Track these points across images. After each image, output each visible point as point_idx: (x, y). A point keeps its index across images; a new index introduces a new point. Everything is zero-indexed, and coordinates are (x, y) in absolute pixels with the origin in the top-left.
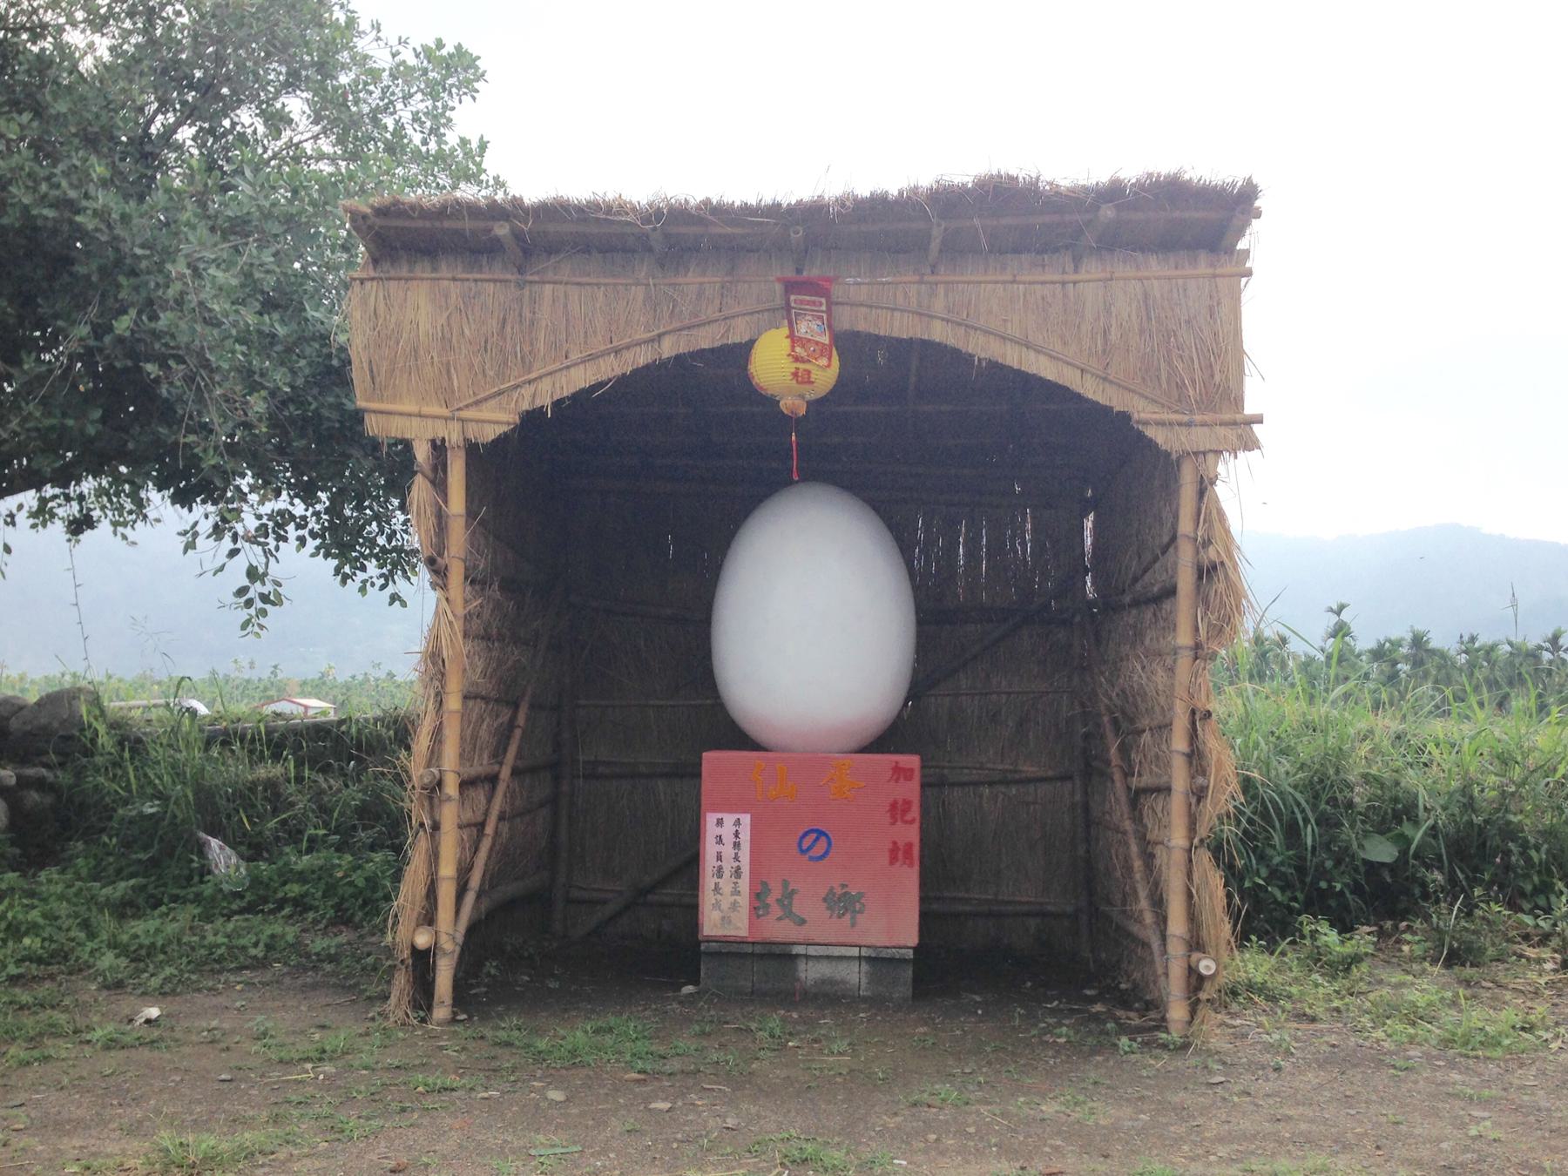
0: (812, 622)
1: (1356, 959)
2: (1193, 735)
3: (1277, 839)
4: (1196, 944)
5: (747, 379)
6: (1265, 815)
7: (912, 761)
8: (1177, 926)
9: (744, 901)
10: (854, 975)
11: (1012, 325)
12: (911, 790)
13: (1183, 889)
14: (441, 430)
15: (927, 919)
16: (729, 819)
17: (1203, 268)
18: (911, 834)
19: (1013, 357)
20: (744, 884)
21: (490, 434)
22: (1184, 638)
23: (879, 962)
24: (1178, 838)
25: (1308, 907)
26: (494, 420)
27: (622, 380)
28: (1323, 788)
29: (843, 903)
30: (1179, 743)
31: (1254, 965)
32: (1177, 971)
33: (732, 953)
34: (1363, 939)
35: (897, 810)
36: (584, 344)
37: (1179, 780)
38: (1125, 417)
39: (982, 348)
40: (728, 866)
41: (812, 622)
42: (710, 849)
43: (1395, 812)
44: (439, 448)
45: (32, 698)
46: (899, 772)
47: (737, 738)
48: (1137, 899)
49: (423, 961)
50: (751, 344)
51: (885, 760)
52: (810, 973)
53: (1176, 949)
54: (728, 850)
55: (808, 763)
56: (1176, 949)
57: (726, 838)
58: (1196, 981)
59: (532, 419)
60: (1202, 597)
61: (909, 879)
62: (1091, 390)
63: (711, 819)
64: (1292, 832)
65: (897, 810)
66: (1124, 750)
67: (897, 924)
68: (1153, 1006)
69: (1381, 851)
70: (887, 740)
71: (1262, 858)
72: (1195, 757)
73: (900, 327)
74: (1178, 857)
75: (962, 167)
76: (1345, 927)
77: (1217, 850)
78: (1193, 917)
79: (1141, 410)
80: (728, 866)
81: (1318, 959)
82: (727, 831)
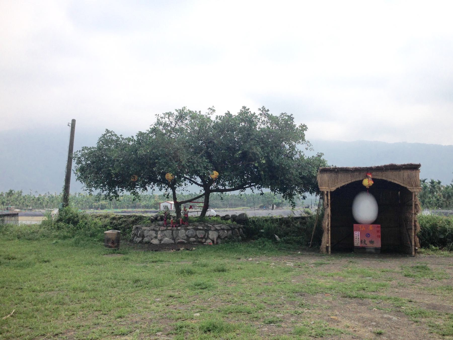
0: (366, 209)
1: (437, 250)
2: (415, 223)
3: (427, 235)
4: (415, 246)
5: (362, 185)
6: (425, 232)
7: (380, 225)
8: (413, 244)
9: (359, 242)
10: (373, 251)
11: (392, 178)
12: (379, 229)
13: (415, 240)
14: (328, 190)
15: (382, 245)
16: (357, 232)
17: (415, 171)
18: (380, 234)
19: (393, 181)
20: (359, 240)
21: (333, 190)
22: (413, 212)
23: (376, 249)
24: (413, 234)
25: (431, 244)
26: (333, 189)
27: (348, 184)
28: (434, 227)
29: (372, 242)
30: (413, 224)
31: (423, 250)
32: (413, 249)
33: (358, 248)
34: (438, 248)
35: (378, 231)
36: (343, 181)
37: (413, 228)
38: (406, 188)
39: (389, 180)
40: (357, 238)
41: (366, 209)
42: (355, 236)
43: (444, 230)
44: (327, 192)
45: (238, 215)
46: (378, 227)
47: (357, 223)
48: (408, 241)
49: (327, 248)
50: (363, 180)
51: (376, 225)
52: (368, 250)
53: (413, 246)
54: (357, 236)
55: (367, 225)
56: (413, 246)
57: (357, 234)
58: (416, 250)
59: (338, 189)
60: (416, 208)
61: (380, 239)
62: (402, 185)
63: (355, 232)
64: (429, 234)
65: (378, 231)
66: (406, 224)
67: (378, 244)
68: (411, 253)
69: (442, 237)
70: (375, 223)
71: (425, 237)
72: (415, 226)
73: (380, 178)
74: (413, 236)
75: (388, 163)
76: (435, 246)
77: (417, 235)
78: (415, 243)
79: (408, 187)
80: (357, 238)
81: (433, 250)
82: (357, 234)
